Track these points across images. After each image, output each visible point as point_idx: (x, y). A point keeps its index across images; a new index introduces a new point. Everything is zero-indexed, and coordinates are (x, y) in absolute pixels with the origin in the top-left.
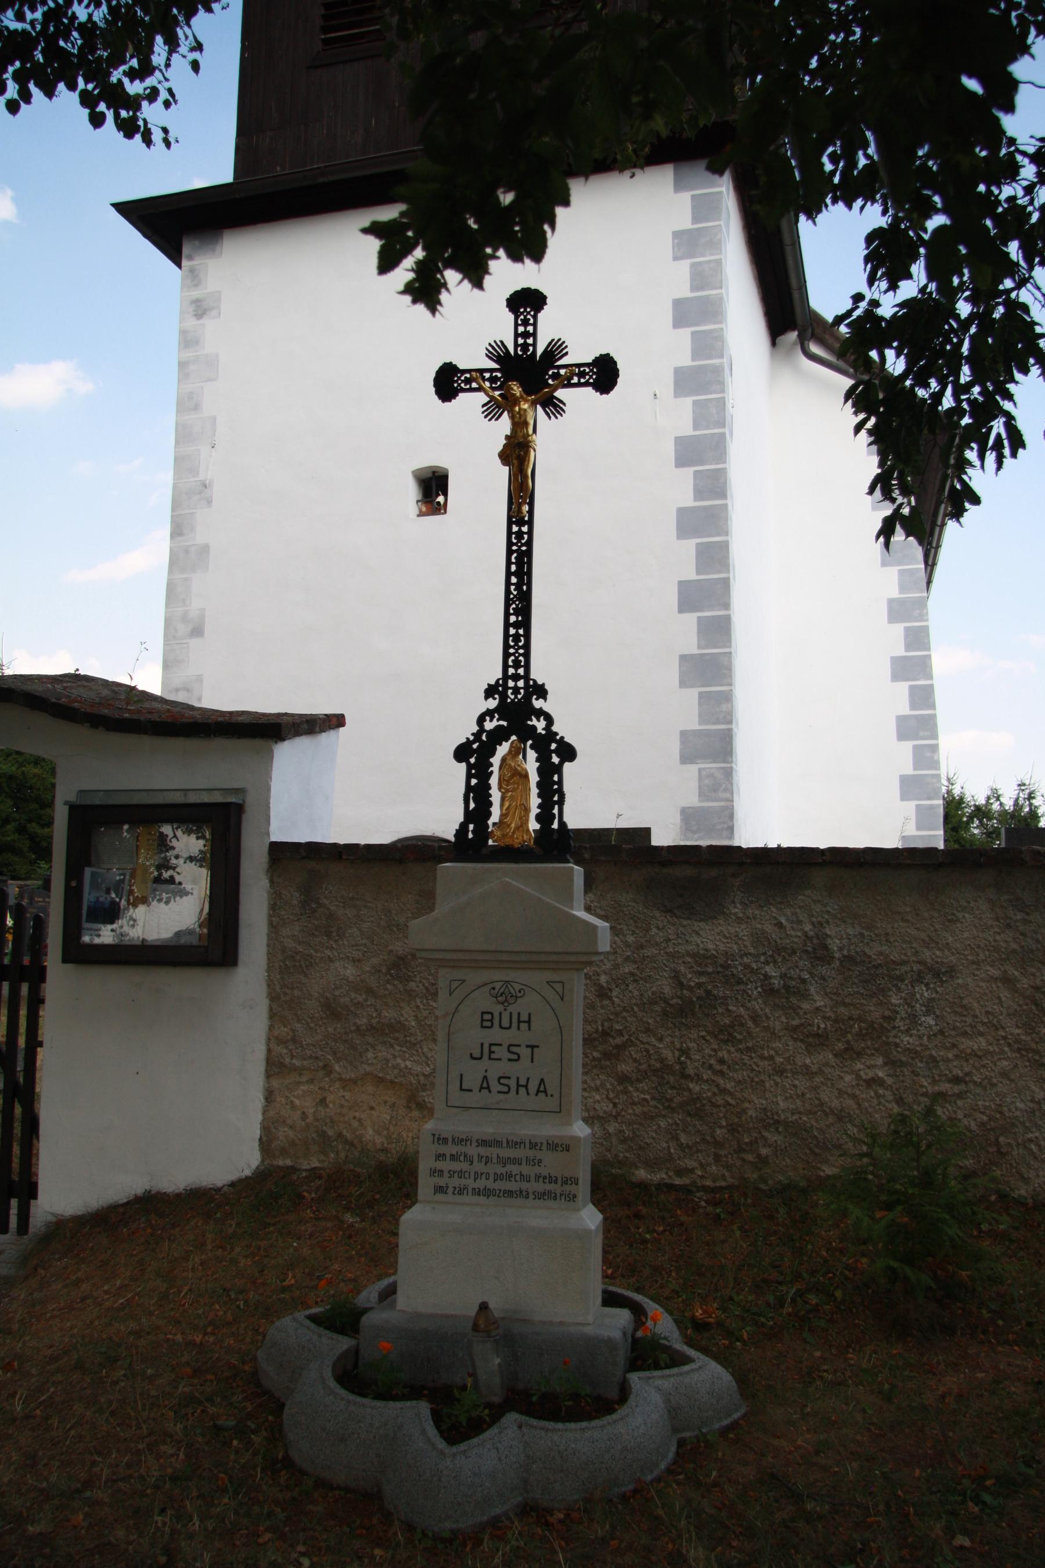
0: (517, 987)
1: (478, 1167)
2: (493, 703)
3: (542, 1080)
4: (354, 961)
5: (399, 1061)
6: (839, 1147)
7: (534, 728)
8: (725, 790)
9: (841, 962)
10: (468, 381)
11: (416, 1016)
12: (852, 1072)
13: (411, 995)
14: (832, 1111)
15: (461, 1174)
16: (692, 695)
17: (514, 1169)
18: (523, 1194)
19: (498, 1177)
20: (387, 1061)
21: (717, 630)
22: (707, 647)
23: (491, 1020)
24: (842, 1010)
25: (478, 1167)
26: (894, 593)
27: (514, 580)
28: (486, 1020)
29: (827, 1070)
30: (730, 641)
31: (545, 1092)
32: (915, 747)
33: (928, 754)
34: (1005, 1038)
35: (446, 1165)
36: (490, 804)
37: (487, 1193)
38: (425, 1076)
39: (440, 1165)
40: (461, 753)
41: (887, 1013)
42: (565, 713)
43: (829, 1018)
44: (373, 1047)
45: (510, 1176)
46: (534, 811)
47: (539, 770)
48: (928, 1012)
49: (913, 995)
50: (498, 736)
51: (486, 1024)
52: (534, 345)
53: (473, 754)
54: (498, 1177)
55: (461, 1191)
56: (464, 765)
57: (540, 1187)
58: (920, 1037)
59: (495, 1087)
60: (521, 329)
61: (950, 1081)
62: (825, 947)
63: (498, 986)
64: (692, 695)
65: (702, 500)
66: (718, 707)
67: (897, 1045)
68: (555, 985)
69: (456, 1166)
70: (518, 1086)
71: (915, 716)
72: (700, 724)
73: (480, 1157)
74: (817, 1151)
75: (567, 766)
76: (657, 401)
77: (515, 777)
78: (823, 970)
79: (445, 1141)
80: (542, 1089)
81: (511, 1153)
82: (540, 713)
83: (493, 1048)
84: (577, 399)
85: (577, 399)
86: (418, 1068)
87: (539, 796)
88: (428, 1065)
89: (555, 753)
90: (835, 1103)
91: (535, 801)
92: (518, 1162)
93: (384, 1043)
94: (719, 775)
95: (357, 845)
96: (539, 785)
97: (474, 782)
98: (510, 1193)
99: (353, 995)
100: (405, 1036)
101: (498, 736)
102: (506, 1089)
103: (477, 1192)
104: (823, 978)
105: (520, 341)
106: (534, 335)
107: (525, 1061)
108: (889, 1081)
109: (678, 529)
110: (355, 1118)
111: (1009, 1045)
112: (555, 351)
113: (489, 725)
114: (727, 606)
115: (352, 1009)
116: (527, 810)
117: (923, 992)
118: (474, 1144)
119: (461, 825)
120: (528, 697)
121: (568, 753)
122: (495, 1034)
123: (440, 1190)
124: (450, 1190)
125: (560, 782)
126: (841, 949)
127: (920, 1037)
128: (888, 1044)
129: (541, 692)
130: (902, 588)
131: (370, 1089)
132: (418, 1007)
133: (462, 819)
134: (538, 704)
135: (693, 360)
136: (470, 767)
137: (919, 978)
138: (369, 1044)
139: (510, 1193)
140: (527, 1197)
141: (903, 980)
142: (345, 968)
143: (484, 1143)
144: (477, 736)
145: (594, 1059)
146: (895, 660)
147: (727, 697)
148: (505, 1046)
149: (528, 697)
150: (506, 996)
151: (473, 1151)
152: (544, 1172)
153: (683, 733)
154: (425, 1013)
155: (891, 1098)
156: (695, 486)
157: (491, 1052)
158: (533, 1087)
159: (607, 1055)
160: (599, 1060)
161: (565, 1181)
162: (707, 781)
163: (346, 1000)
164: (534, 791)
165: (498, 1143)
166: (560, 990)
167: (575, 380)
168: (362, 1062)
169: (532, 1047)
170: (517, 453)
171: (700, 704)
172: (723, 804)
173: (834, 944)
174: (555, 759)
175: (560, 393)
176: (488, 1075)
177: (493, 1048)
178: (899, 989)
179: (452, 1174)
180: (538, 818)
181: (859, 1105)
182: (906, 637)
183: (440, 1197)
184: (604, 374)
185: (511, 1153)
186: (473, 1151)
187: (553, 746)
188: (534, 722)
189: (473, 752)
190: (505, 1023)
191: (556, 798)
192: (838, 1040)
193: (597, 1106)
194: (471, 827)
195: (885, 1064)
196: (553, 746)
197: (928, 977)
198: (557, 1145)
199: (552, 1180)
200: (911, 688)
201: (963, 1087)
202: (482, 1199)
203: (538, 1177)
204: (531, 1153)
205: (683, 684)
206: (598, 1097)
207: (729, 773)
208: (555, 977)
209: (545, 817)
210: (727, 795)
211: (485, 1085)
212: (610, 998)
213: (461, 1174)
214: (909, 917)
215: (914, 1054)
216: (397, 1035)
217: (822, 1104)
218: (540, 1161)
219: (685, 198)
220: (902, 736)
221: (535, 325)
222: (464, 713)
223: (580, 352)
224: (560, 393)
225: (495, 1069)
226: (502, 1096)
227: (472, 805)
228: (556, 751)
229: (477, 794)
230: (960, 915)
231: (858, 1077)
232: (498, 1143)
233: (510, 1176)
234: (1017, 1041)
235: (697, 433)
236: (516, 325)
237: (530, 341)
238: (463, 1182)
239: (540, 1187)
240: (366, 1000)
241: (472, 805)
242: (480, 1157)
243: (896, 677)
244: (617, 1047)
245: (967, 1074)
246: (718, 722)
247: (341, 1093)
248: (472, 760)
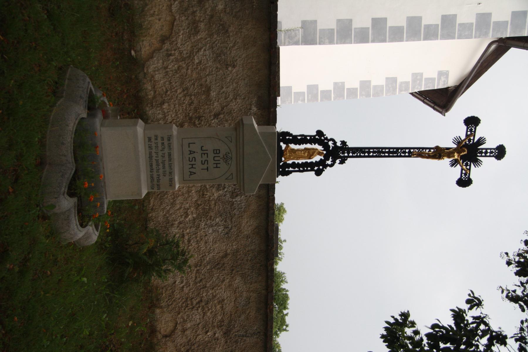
0: (230, 162)
1: (160, 154)
2: (339, 144)
3: (195, 173)
4: (225, 8)
5: (182, 32)
7: (328, 160)
8: (289, 42)
9: (231, 201)
10: (471, 131)
11: (202, 38)
12: (190, 207)
13: (211, 35)
14: (175, 201)
15: (157, 147)
16: (333, 26)
17: (161, 166)
18: (152, 170)
19: (157, 161)
20: (182, 26)
21: (362, 37)
22: (355, 32)
23: (217, 153)
24: (213, 202)
25: (160, 154)
28: (216, 152)
30: (357, 43)
31: (191, 175)
32: (304, 93)
33: (301, 98)
34: (205, 255)
35: (159, 141)
36: (300, 145)
37: (151, 157)
38: (177, 44)
39: (159, 139)
40: (320, 133)
41: (212, 218)
42: (335, 172)
43: (210, 198)
44: (187, 19)
45: (158, 165)
46: (296, 162)
47: (312, 162)
48: (214, 231)
49: (220, 226)
50: (326, 147)
51: (215, 151)
52: (481, 156)
53: (319, 138)
54: (157, 161)
55: (150, 147)
56: (315, 134)
57: (155, 176)
58: (204, 228)
59: (191, 156)
60: (489, 151)
61: (189, 239)
62: (237, 196)
63: (230, 155)
64: (333, 26)
65: (424, 29)
66: (329, 37)
67: (201, 221)
68: (231, 177)
69: (160, 145)
70: (192, 165)
71: (318, 93)
72: (320, 30)
73: (164, 154)
74: (159, 196)
75: (314, 172)
76: (476, 5)
78: (228, 196)
79: (169, 140)
80: (192, 173)
81: (167, 165)
82: (334, 162)
83: (206, 155)
86: (179, 41)
87: (302, 163)
88: (181, 45)
89: (319, 169)
90: (178, 202)
91: (300, 161)
92: (164, 167)
93: (189, 24)
94: (295, 40)
95: (277, 10)
96: (306, 162)
97: (308, 138)
98: (151, 165)
99: (210, 9)
101: (326, 147)
102: (191, 160)
103: (150, 153)
104: (225, 195)
105: (484, 151)
106: (486, 156)
108: (187, 219)
109: (412, 17)
111: (203, 257)
112: (481, 141)
113: (331, 143)
114: (373, 41)
115: (203, 9)
117: (221, 229)
118: (169, 151)
119: (292, 134)
120: (340, 157)
121: (319, 173)
122: (211, 155)
123: (150, 139)
124: (150, 143)
125: (307, 171)
126: (236, 201)
127: (204, 228)
128: (201, 218)
130: (375, 87)
131: (168, 18)
132: (206, 39)
133: (294, 134)
134: (338, 161)
136: (314, 136)
137: (226, 227)
138: (188, 17)
139: (151, 165)
140: (151, 172)
141: (225, 222)
142: (222, 5)
143: (170, 155)
144: (326, 139)
145: (189, 114)
146: (343, 84)
147: (331, 42)
148: (207, 159)
149: (340, 157)
150: (226, 158)
151: (166, 151)
152: (161, 178)
153: (316, 21)
154: (204, 42)
155: (181, 220)
156: (431, 25)
157: (204, 154)
158: (192, 170)
159: (191, 119)
160: (189, 116)
161: (158, 185)
162: (293, 33)
163: (207, 6)
164: (304, 161)
165: (170, 160)
166: (229, 178)
168: (180, 14)
169: (207, 169)
170: (438, 153)
171: (329, 29)
172: (283, 41)
173: (238, 199)
174: (316, 168)
176: (196, 153)
177: (206, 155)
178: (222, 221)
179: (156, 143)
180: (294, 163)
181: (178, 210)
182: (353, 89)
183: (147, 140)
184: (464, 182)
185: (167, 165)
186: (166, 151)
187: (321, 167)
188: (331, 160)
189: (320, 137)
190: (216, 159)
191: (301, 169)
192: (202, 202)
193: (169, 116)
194: (291, 138)
195: (194, 217)
197: (226, 230)
198: (171, 182)
199: (158, 180)
200: (331, 91)
201: (187, 243)
202: (148, 156)
203: (159, 175)
204: (168, 173)
205: (339, 21)
206: (173, 116)
207: (297, 43)
208: (234, 175)
209: (294, 165)
210: (287, 43)
211: (191, 152)
212: (214, 119)
213: (157, 147)
214: (249, 223)
215: (198, 227)
216: (193, 30)
217: (177, 197)
218: (165, 176)
220: (310, 87)
221: (490, 156)
222: (336, 134)
223: (475, 172)
225: (198, 156)
226: (188, 159)
227: (299, 138)
228: (319, 169)
230: (250, 240)
231: (188, 209)
232: (170, 160)
233: (158, 165)
234: (204, 260)
236: (491, 149)
237: (483, 154)
238: (154, 148)
239: (155, 176)
240: (208, 15)
241: (299, 138)
242: (164, 154)
243: (335, 84)
244: (195, 123)
245: (191, 245)
246: (320, 38)
247: (165, 5)
248: (317, 137)
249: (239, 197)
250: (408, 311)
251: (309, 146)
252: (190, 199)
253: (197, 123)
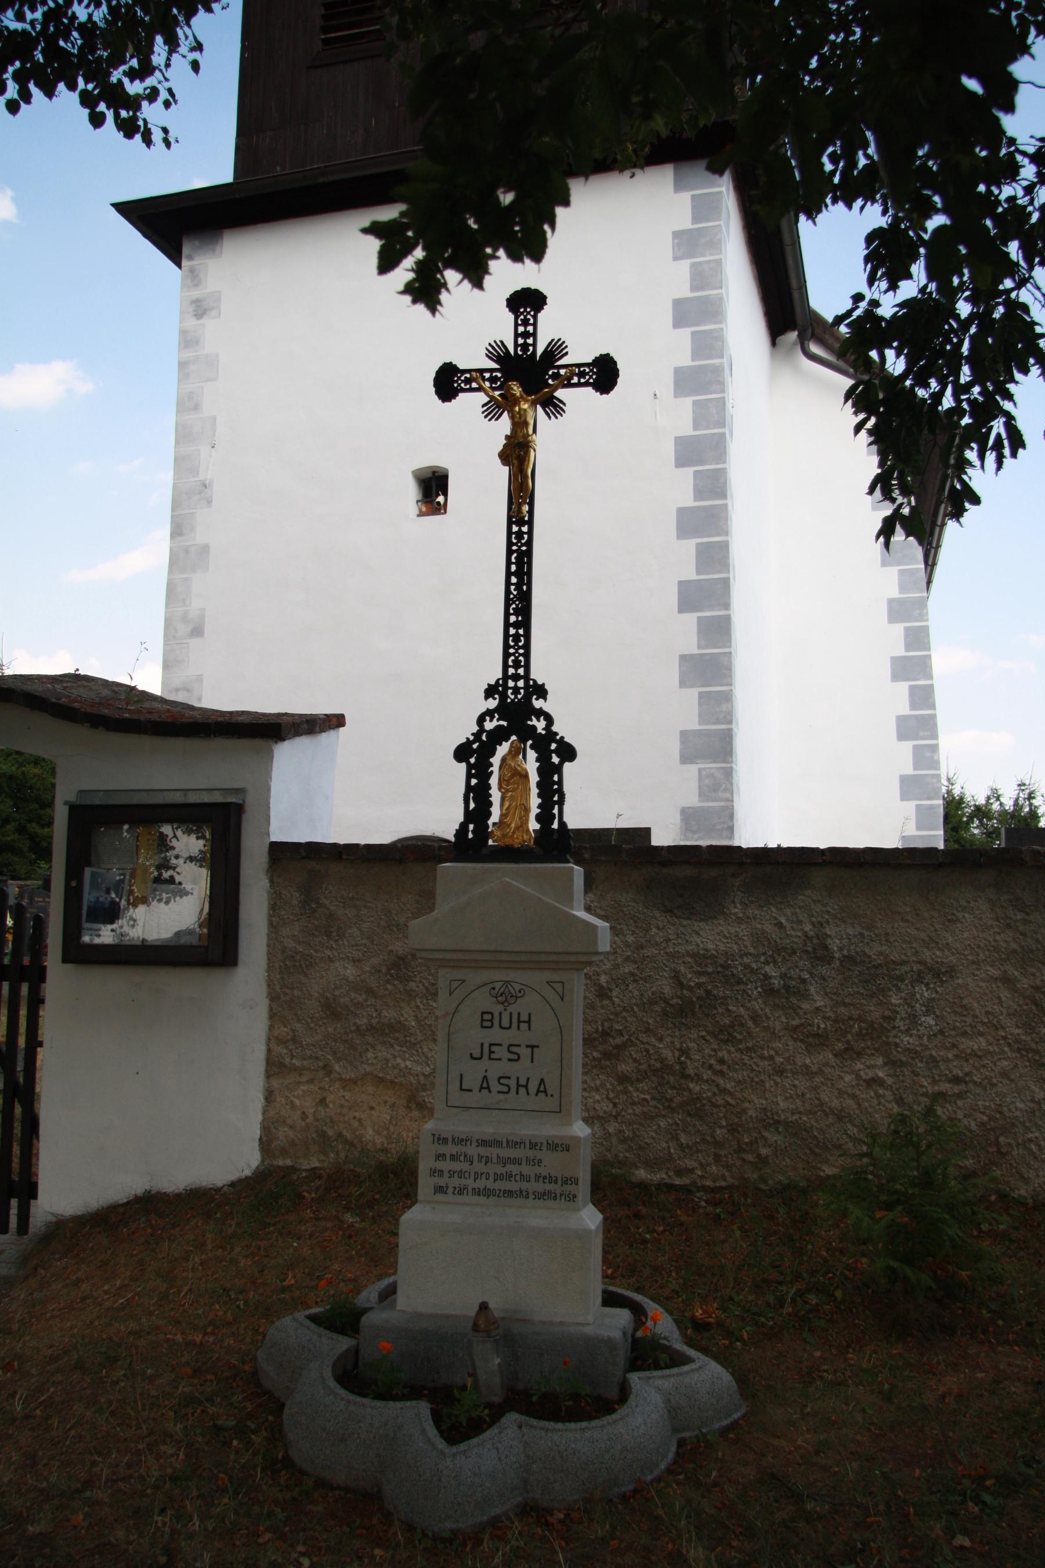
0: (517, 987)
1: (478, 1167)
2: (493, 703)
3: (542, 1080)
4: (354, 961)
5: (399, 1061)
7: (534, 728)
8: (725, 790)
9: (841, 962)
10: (468, 381)
11: (416, 1016)
12: (852, 1072)
13: (411, 995)
14: (832, 1111)
15: (461, 1174)
16: (692, 695)
17: (514, 1169)
18: (523, 1194)
19: (498, 1177)
20: (387, 1061)
21: (717, 630)
22: (707, 647)
23: (491, 1020)
24: (842, 1010)
25: (478, 1167)
26: (894, 593)
27: (514, 580)
28: (486, 1020)
30: (730, 641)
31: (545, 1092)
32: (915, 747)
33: (928, 754)
35: (446, 1165)
36: (490, 804)
37: (487, 1193)
38: (425, 1076)
39: (440, 1165)
40: (461, 753)
41: (887, 1013)
42: (565, 713)
43: (829, 1018)
44: (373, 1047)
45: (510, 1176)
46: (534, 811)
47: (539, 770)
48: (928, 1012)
49: (913, 995)
50: (498, 736)
51: (486, 1024)
52: (534, 345)
53: (473, 754)
54: (498, 1177)
55: (461, 1191)
56: (464, 765)
57: (540, 1187)
58: (920, 1037)
59: (495, 1087)
60: (521, 329)
61: (950, 1081)
62: (825, 947)
63: (498, 986)
64: (692, 695)
65: (702, 500)
66: (718, 707)
67: (897, 1045)
68: (555, 985)
69: (456, 1166)
70: (518, 1086)
71: (915, 716)
72: (700, 724)
73: (480, 1157)
74: (817, 1151)
75: (567, 766)
77: (515, 777)
78: (823, 970)
79: (445, 1141)
80: (542, 1089)
81: (511, 1153)
82: (540, 713)
83: (493, 1048)
84: (577, 399)
85: (577, 399)
86: (418, 1068)
87: (539, 796)
88: (428, 1065)
89: (555, 753)
90: (835, 1103)
91: (535, 801)
92: (518, 1162)
93: (384, 1043)
94: (719, 775)
95: (357, 845)
96: (539, 785)
97: (474, 782)
98: (510, 1193)
99: (353, 995)
100: (405, 1036)
101: (498, 736)
102: (506, 1089)
103: (477, 1192)
104: (823, 978)
105: (520, 341)
106: (534, 335)
107: (525, 1061)
108: (889, 1081)
109: (678, 529)
110: (355, 1118)
111: (1009, 1045)
112: (555, 351)
113: (489, 725)
114: (727, 606)
115: (352, 1009)
116: (527, 810)
117: (923, 992)
118: (474, 1144)
119: (461, 825)
120: (528, 697)
121: (568, 753)
122: (495, 1034)
123: (440, 1190)
124: (450, 1190)
125: (560, 782)
126: (841, 949)
127: (920, 1037)
128: (888, 1044)
129: (541, 692)
130: (902, 588)
131: (370, 1089)
132: (418, 1007)
133: (462, 819)
134: (538, 704)
135: (693, 360)
136: (470, 767)
137: (919, 978)
138: (369, 1044)
139: (510, 1193)
140: (527, 1197)
141: (903, 980)
142: (345, 968)
143: (484, 1143)
144: (477, 736)
145: (594, 1059)
146: (895, 660)
147: (727, 697)
148: (505, 1046)
149: (528, 697)
150: (506, 996)
151: (473, 1151)
152: (544, 1172)
153: (683, 733)
154: (425, 1013)
155: (891, 1098)
156: (695, 486)
157: (491, 1052)
158: (533, 1087)
159: (607, 1055)
160: (599, 1060)
161: (565, 1181)
162: (707, 781)
163: (346, 1000)
164: (534, 791)
165: (498, 1143)
166: (560, 990)
167: (575, 380)
168: (362, 1062)
169: (532, 1047)
170: (517, 453)
171: (700, 704)
172: (723, 804)
173: (834, 944)
174: (555, 759)
175: (560, 393)
176: (488, 1075)
177: (493, 1048)
178: (899, 989)
179: (452, 1174)
180: (538, 818)
181: (859, 1105)
182: (906, 637)
183: (440, 1197)
184: (604, 374)
185: (511, 1153)
186: (473, 1151)
187: (553, 746)
188: (534, 722)
189: (473, 752)
190: (505, 1023)
191: (556, 798)
192: (838, 1040)
193: (597, 1106)
194: (471, 827)
195: (885, 1064)
196: (553, 746)
197: (928, 977)
198: (557, 1145)
199: (552, 1180)
200: (911, 688)
201: (963, 1087)
202: (482, 1199)
203: (538, 1177)
204: (531, 1153)
205: (683, 684)
206: (598, 1097)
207: (729, 773)
208: (555, 977)
209: (545, 817)
210: (727, 795)
211: (485, 1085)
212: (610, 998)
213: (461, 1174)
214: (909, 917)
215: (914, 1054)
216: (397, 1035)
217: (822, 1104)
218: (540, 1161)
219: (685, 198)
220: (902, 736)
221: (535, 325)
222: (464, 713)
223: (580, 352)
224: (560, 393)
225: (495, 1069)
226: (502, 1096)
227: (472, 805)
228: (556, 751)
229: (477, 794)
231: (858, 1077)
232: (498, 1143)
233: (510, 1176)
234: (1017, 1041)
235: (697, 433)
236: (516, 325)
237: (530, 341)
238: (463, 1182)
239: (540, 1187)
240: (366, 1000)
241: (472, 805)
242: (480, 1157)
243: (896, 677)
244: (617, 1047)
245: (967, 1074)
246: (718, 722)
247: (341, 1093)
248: (472, 760)
249: (829, 941)
250: (871, 491)
251: (494, 781)
252: (827, 1070)
253: (618, 1040)
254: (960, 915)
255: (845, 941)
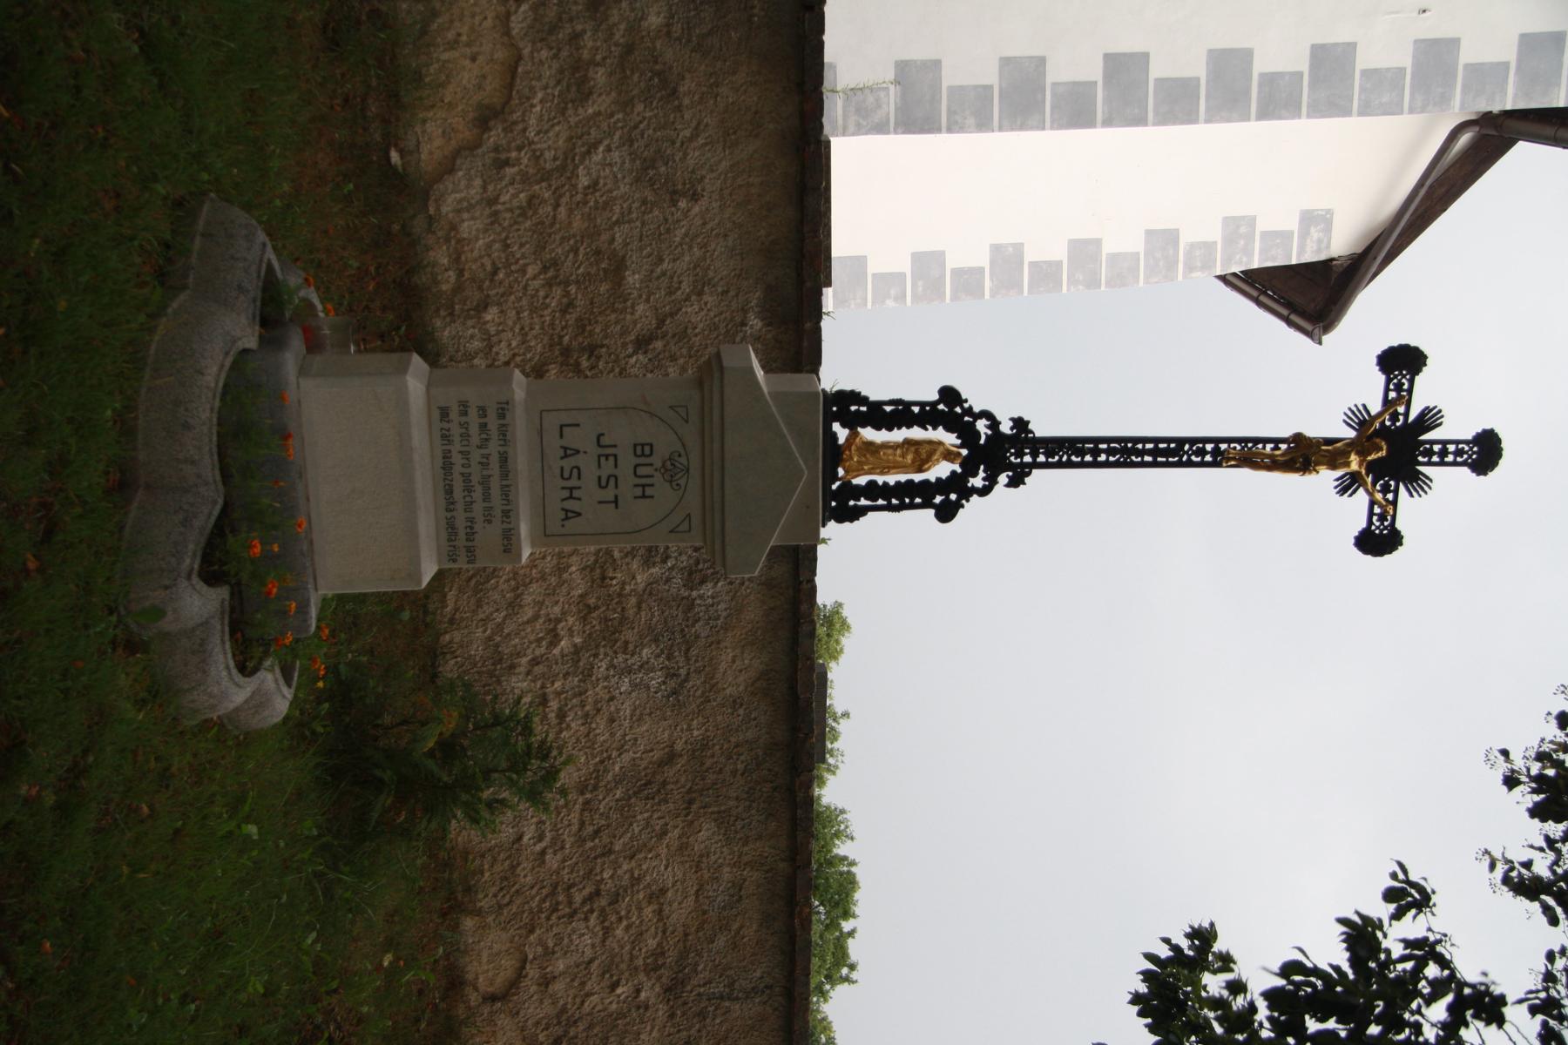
0: (682, 482)
1: (476, 456)
2: (1006, 428)
3: (579, 514)
4: (668, 25)
5: (540, 95)
6: (479, 605)
7: (975, 475)
8: (858, 125)
9: (686, 598)
10: (1399, 388)
11: (599, 113)
12: (563, 613)
13: (626, 105)
14: (518, 596)
15: (466, 436)
16: (990, 76)
17: (478, 494)
18: (450, 505)
19: (466, 478)
20: (539, 78)
21: (1076, 110)
22: (1054, 95)
23: (643, 455)
24: (633, 600)
25: (476, 456)
28: (643, 450)
29: (564, 590)
30: (1060, 127)
31: (567, 518)
32: (903, 275)
33: (893, 292)
34: (609, 758)
35: (473, 418)
36: (890, 429)
37: (447, 466)
38: (525, 130)
39: (473, 412)
40: (949, 395)
41: (631, 647)
42: (995, 510)
43: (623, 588)
44: (556, 56)
45: (469, 490)
46: (880, 480)
47: (926, 482)
48: (635, 686)
49: (653, 670)
50: (968, 436)
51: (639, 449)
52: (1429, 464)
53: (948, 409)
54: (466, 478)
55: (446, 437)
56: (936, 397)
57: (461, 523)
58: (606, 678)
59: (568, 464)
60: (1451, 448)
61: (560, 709)
62: (703, 582)
63: (683, 460)
64: (990, 76)
65: (1260, 85)
66: (976, 111)
67: (596, 656)
68: (686, 524)
69: (474, 429)
70: (571, 489)
71: (943, 276)
72: (950, 88)
73: (487, 456)
74: (473, 582)
75: (932, 512)
76: (1415, 14)
78: (678, 581)
79: (502, 416)
80: (569, 515)
81: (495, 491)
82: (991, 481)
83: (611, 459)
86: (533, 121)
87: (898, 483)
88: (538, 133)
89: (946, 501)
90: (528, 599)
91: (891, 479)
92: (487, 497)
93: (561, 71)
94: (877, 117)
95: (822, 31)
96: (910, 482)
97: (916, 409)
98: (449, 491)
99: (622, 27)
100: (573, 101)
101: (968, 436)
102: (566, 475)
103: (447, 456)
104: (668, 580)
105: (1436, 448)
106: (1442, 463)
108: (556, 651)
109: (1224, 51)
110: (459, 35)
111: (602, 762)
112: (1429, 419)
113: (982, 425)
114: (1108, 122)
115: (603, 27)
117: (656, 679)
118: (502, 449)
119: (866, 398)
120: (1011, 467)
121: (946, 514)
122: (627, 461)
123: (444, 413)
124: (445, 425)
125: (912, 506)
126: (701, 597)
127: (606, 678)
128: (597, 647)
130: (1114, 258)
131: (500, 55)
132: (612, 115)
133: (872, 398)
134: (1003, 479)
136: (934, 404)
137: (671, 675)
138: (559, 50)
139: (449, 491)
140: (448, 510)
141: (668, 659)
142: (659, 13)
143: (504, 459)
144: (969, 411)
145: (561, 337)
146: (1019, 248)
147: (983, 125)
148: (616, 472)
149: (1011, 467)
150: (672, 470)
151: (494, 448)
152: (477, 527)
153: (937, 64)
154: (604, 125)
155: (537, 653)
156: (1281, 75)
157: (607, 457)
158: (569, 505)
159: (566, 352)
160: (560, 343)
161: (470, 550)
162: (871, 99)
163: (615, 18)
164: (903, 478)
165: (505, 474)
166: (681, 528)
168: (534, 43)
169: (616, 501)
170: (1301, 454)
171: (976, 87)
172: (840, 122)
173: (707, 590)
174: (938, 499)
176: (581, 456)
177: (611, 459)
178: (658, 656)
179: (465, 426)
180: (872, 483)
181: (528, 622)
182: (1049, 263)
183: (436, 414)
184: (1379, 540)
185: (495, 491)
186: (494, 448)
187: (953, 497)
188: (982, 474)
189: (951, 408)
190: (642, 471)
191: (894, 501)
192: (598, 598)
193: (503, 344)
194: (864, 409)
195: (575, 645)
197: (672, 683)
198: (509, 539)
199: (470, 536)
200: (982, 270)
201: (554, 721)
202: (439, 462)
203: (471, 520)
204: (498, 512)
205: (1006, 62)
206: (514, 344)
207: (881, 128)
208: (696, 520)
209: (872, 490)
210: (851, 128)
211: (568, 452)
212: (635, 353)
213: (466, 436)
214: (738, 663)
215: (588, 674)
216: (574, 89)
217: (526, 585)
218: (490, 522)
220: (919, 259)
221: (1455, 464)
222: (997, 397)
223: (1410, 511)
225: (587, 462)
226: (558, 471)
227: (888, 409)
228: (947, 501)
231: (558, 621)
232: (505, 474)
233: (469, 490)
234: (606, 771)
236: (1457, 442)
237: (1435, 459)
238: (457, 439)
239: (461, 523)
240: (616, 45)
241: (888, 409)
242: (487, 456)
243: (996, 249)
244: (578, 364)
245: (568, 727)
246: (950, 112)
247: (490, 15)
248: (941, 407)
254: (741, 711)
255: (710, 601)
